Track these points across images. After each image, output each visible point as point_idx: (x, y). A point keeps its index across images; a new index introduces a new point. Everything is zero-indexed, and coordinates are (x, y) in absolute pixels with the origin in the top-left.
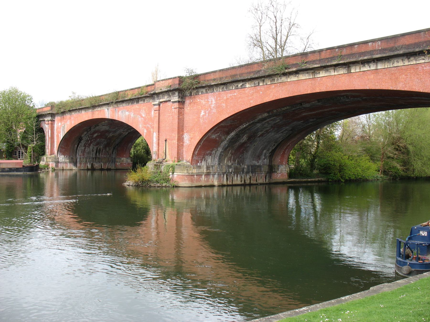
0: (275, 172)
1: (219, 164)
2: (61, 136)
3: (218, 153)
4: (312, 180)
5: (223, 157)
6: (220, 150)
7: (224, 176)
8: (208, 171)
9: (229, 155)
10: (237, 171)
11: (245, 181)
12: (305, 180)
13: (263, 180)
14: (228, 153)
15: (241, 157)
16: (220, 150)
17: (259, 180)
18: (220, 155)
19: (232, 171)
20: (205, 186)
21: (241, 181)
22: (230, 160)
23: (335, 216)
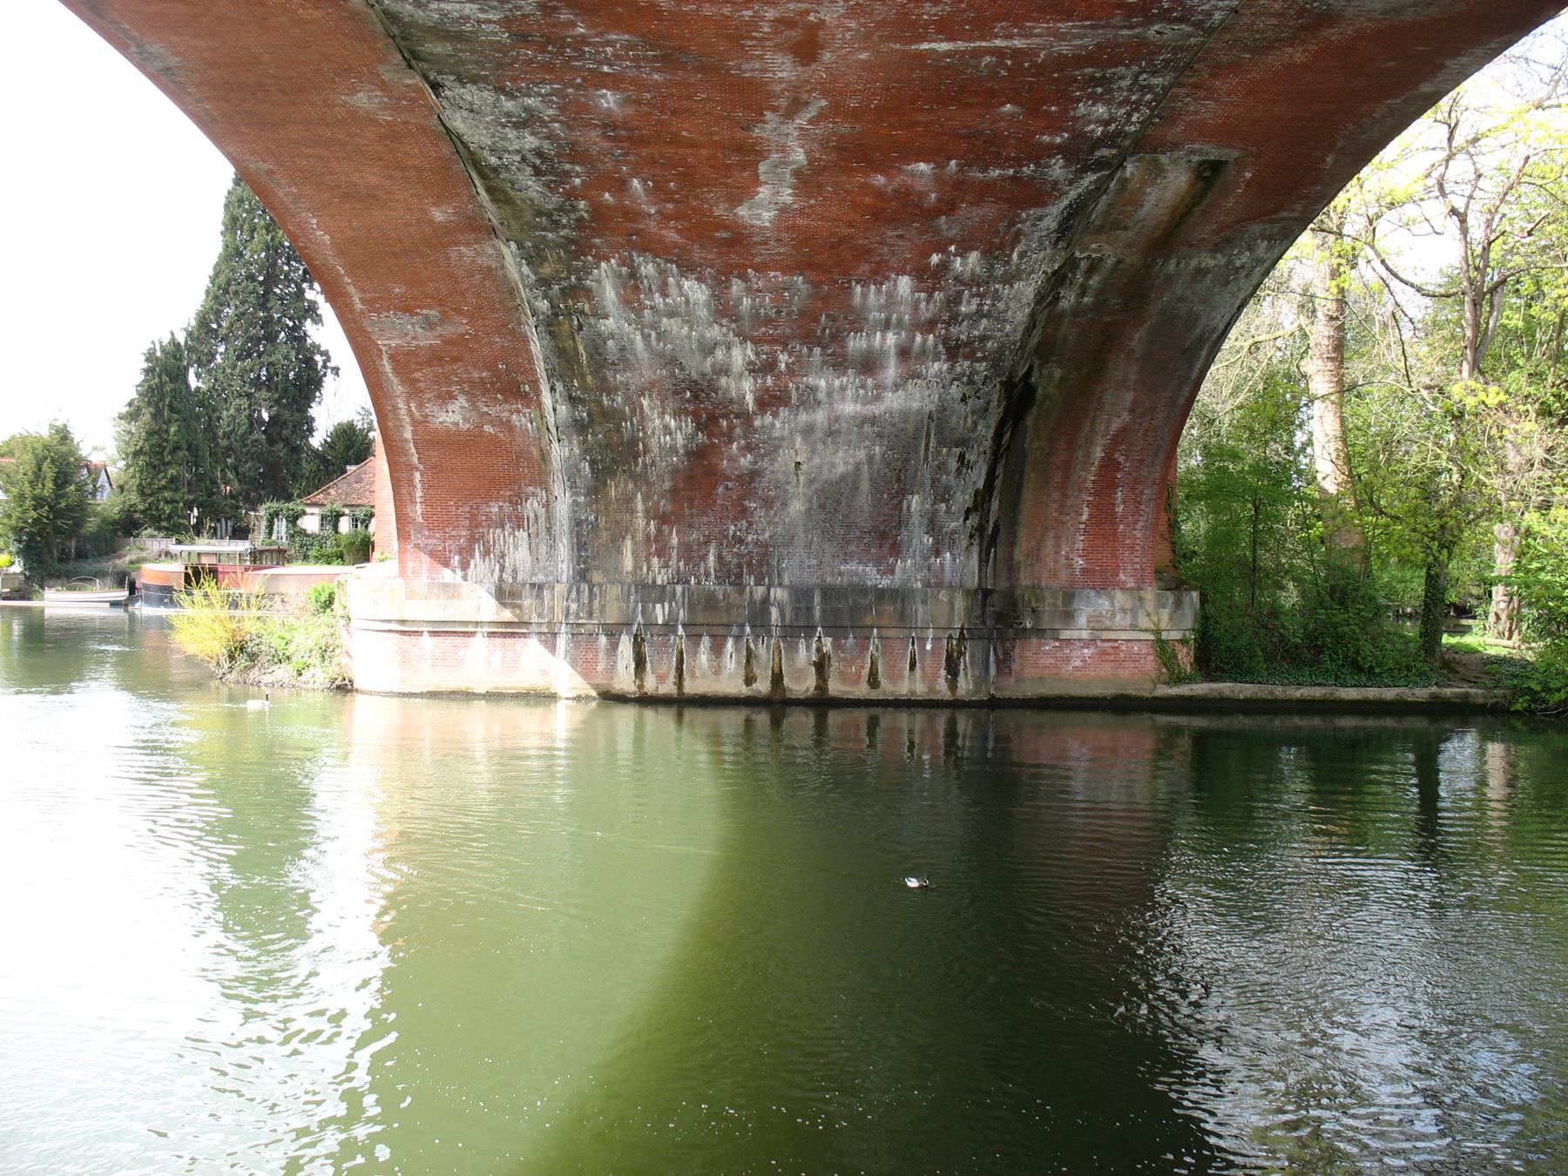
0: (1040, 632)
1: (582, 575)
4: (1372, 693)
7: (613, 647)
10: (709, 621)
11: (777, 678)
12: (1317, 692)
13: (931, 680)
17: (895, 677)
20: (494, 697)
21: (749, 680)
23: (678, 818)
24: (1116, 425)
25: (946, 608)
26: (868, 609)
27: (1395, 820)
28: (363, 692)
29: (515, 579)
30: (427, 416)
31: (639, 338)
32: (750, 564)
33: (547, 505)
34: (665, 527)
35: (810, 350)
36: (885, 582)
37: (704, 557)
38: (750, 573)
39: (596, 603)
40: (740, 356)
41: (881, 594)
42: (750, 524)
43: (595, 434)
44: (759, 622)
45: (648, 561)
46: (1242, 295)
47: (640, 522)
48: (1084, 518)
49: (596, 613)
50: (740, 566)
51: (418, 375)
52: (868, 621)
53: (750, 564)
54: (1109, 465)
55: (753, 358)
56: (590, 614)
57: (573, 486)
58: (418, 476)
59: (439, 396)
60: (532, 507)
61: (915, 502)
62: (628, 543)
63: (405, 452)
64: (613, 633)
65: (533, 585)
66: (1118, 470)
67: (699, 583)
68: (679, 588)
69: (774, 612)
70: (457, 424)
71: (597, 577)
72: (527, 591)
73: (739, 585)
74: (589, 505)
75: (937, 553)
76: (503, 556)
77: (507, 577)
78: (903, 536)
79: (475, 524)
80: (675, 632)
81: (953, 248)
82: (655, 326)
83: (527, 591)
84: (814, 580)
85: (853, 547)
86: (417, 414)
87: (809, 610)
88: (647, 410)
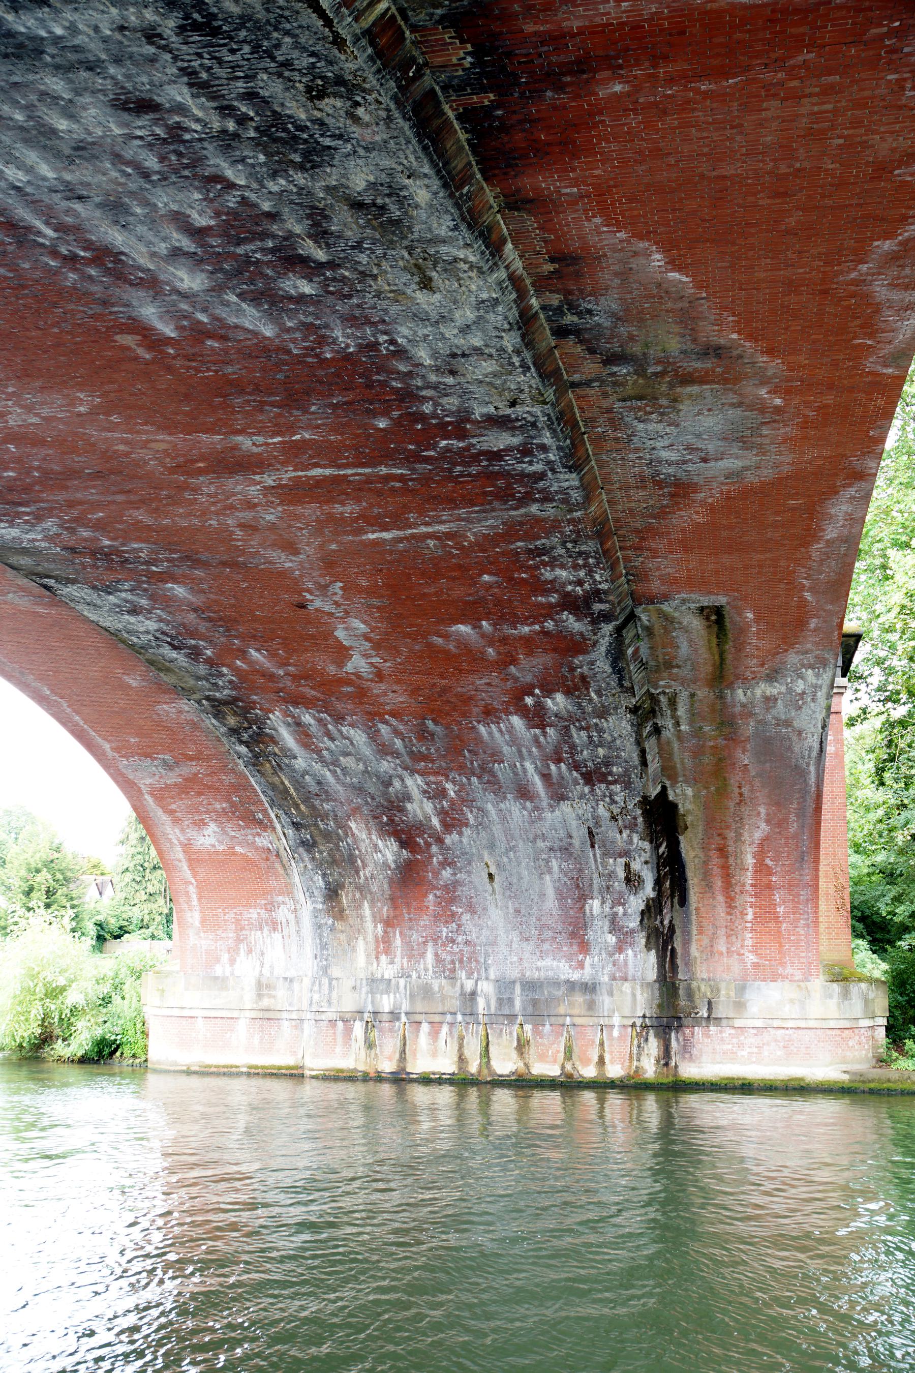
24: (758, 835)
25: (629, 998)
27: (442, 1132)
28: (155, 1071)
29: (272, 973)
30: (189, 840)
31: (328, 773)
33: (295, 911)
34: (389, 929)
35: (469, 779)
36: (575, 976)
37: (423, 955)
38: (462, 968)
39: (334, 994)
40: (414, 784)
41: (572, 986)
42: (459, 926)
43: (321, 853)
44: (468, 1011)
46: (820, 716)
47: (369, 925)
48: (750, 917)
49: (335, 1001)
50: (453, 962)
51: (174, 807)
52: (562, 1010)
53: (461, 961)
54: (761, 869)
55: (425, 787)
57: (312, 895)
59: (194, 823)
61: (595, 905)
65: (286, 979)
66: (771, 874)
67: (419, 977)
68: (402, 982)
70: (214, 846)
73: (452, 978)
78: (591, 935)
80: (398, 1019)
82: (336, 763)
84: (515, 974)
85: (546, 946)
86: (182, 839)
87: (511, 1000)
88: (356, 831)
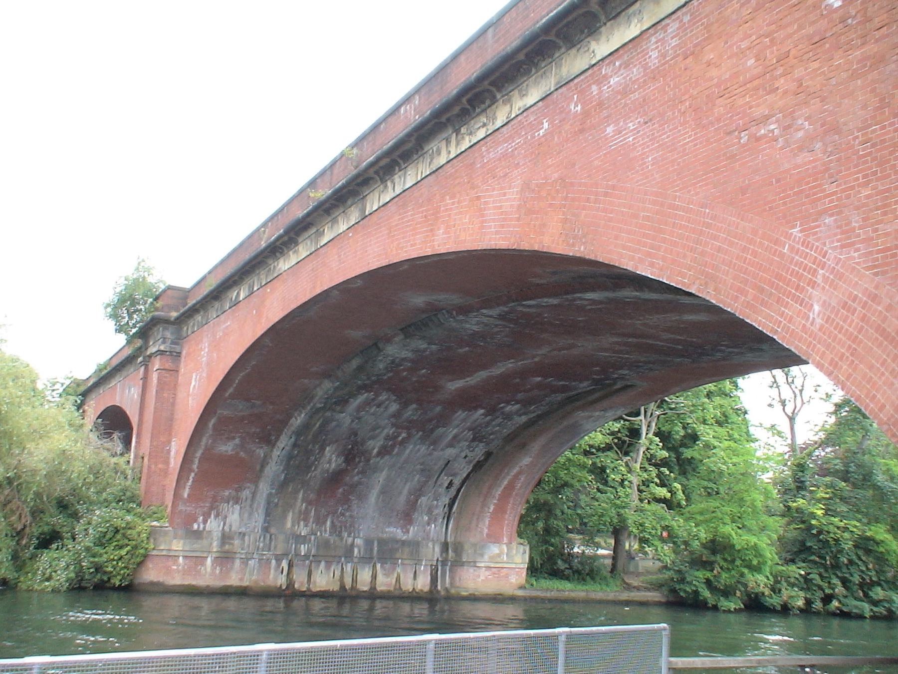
1: (266, 529)
2: (445, 239)
3: (261, 499)
5: (280, 509)
6: (264, 488)
8: (227, 547)
9: (300, 505)
14: (296, 499)
15: (343, 514)
16: (264, 488)
18: (269, 503)
19: (309, 550)
22: (306, 520)
26: (397, 550)
32: (345, 527)
34: (310, 507)
37: (325, 523)
39: (273, 543)
41: (404, 543)
45: (299, 524)
49: (272, 549)
52: (398, 556)
53: (345, 527)
56: (269, 550)
58: (193, 475)
60: (246, 493)
62: (291, 514)
63: (192, 462)
64: (279, 560)
68: (313, 538)
69: (356, 550)
71: (273, 530)
72: (236, 536)
73: (340, 535)
74: (277, 494)
75: (429, 524)
76: (226, 517)
77: (227, 528)
79: (214, 499)
81: (454, 313)
83: (236, 536)
85: (392, 520)
87: (372, 550)
